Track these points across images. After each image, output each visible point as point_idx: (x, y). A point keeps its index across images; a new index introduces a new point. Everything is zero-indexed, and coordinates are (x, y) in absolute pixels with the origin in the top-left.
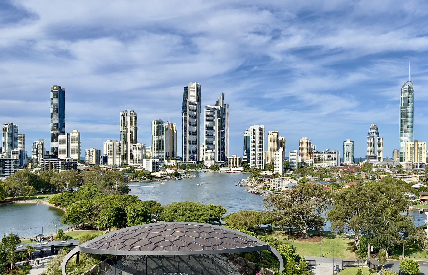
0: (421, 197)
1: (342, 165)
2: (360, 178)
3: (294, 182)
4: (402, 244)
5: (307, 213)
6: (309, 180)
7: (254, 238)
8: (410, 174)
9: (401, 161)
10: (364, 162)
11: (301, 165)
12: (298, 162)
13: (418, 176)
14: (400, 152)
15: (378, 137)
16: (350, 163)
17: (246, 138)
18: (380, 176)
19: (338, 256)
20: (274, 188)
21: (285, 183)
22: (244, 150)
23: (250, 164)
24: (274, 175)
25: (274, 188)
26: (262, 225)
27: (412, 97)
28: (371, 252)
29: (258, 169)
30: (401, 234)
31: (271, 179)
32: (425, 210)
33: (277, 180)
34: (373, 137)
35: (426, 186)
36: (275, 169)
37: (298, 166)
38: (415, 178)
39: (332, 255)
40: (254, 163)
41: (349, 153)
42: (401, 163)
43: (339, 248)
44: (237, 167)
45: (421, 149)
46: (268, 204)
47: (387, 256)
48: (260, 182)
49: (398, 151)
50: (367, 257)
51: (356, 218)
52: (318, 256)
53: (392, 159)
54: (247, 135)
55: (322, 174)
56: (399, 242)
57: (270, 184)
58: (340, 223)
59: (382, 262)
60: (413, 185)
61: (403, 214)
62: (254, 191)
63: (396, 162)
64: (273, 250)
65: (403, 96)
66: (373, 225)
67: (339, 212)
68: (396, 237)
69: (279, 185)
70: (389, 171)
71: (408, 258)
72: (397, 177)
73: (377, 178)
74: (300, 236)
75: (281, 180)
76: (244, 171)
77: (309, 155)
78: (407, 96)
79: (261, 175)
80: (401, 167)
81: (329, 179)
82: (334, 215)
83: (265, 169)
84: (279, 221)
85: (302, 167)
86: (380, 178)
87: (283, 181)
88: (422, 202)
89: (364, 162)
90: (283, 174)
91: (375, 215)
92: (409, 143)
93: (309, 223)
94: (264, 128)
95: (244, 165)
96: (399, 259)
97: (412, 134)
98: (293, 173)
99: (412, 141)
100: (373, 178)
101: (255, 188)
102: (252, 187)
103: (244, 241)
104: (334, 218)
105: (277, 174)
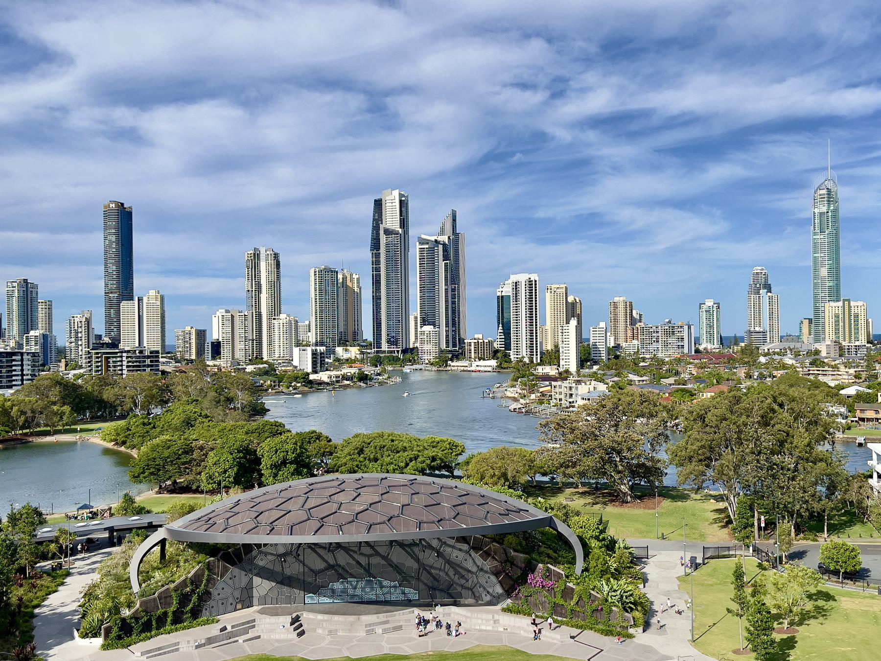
0: (859, 414)
1: (697, 351)
2: (734, 377)
3: (602, 387)
5: (629, 449)
7: (521, 504)
8: (835, 368)
9: (817, 340)
10: (743, 344)
11: (615, 352)
13: (852, 371)
14: (816, 322)
15: (769, 294)
18: (775, 373)
19: (694, 536)
20: (560, 400)
21: (583, 389)
23: (511, 352)
24: (560, 374)
25: (560, 400)
26: (539, 478)
27: (836, 211)
28: (760, 528)
31: (553, 383)
32: (869, 439)
33: (566, 384)
34: (759, 293)
36: (562, 363)
38: (845, 374)
40: (520, 351)
41: (711, 327)
42: (817, 346)
43: (696, 520)
44: (484, 360)
47: (793, 534)
49: (810, 321)
50: (754, 537)
51: (728, 458)
53: (798, 337)
54: (503, 294)
55: (657, 369)
57: (553, 394)
59: (784, 548)
64: (562, 528)
65: (817, 211)
67: (694, 447)
69: (571, 395)
70: (794, 362)
71: (835, 539)
72: (809, 374)
73: (770, 377)
74: (614, 497)
75: (574, 385)
76: (500, 366)
77: (629, 333)
78: (824, 209)
80: (817, 352)
81: (671, 380)
83: (542, 363)
86: (774, 377)
87: (579, 386)
89: (743, 344)
90: (578, 371)
92: (832, 304)
94: (537, 279)
97: (838, 286)
98: (599, 369)
99: (838, 301)
100: (762, 377)
101: (522, 401)
102: (515, 400)
103: (502, 510)
105: (567, 371)
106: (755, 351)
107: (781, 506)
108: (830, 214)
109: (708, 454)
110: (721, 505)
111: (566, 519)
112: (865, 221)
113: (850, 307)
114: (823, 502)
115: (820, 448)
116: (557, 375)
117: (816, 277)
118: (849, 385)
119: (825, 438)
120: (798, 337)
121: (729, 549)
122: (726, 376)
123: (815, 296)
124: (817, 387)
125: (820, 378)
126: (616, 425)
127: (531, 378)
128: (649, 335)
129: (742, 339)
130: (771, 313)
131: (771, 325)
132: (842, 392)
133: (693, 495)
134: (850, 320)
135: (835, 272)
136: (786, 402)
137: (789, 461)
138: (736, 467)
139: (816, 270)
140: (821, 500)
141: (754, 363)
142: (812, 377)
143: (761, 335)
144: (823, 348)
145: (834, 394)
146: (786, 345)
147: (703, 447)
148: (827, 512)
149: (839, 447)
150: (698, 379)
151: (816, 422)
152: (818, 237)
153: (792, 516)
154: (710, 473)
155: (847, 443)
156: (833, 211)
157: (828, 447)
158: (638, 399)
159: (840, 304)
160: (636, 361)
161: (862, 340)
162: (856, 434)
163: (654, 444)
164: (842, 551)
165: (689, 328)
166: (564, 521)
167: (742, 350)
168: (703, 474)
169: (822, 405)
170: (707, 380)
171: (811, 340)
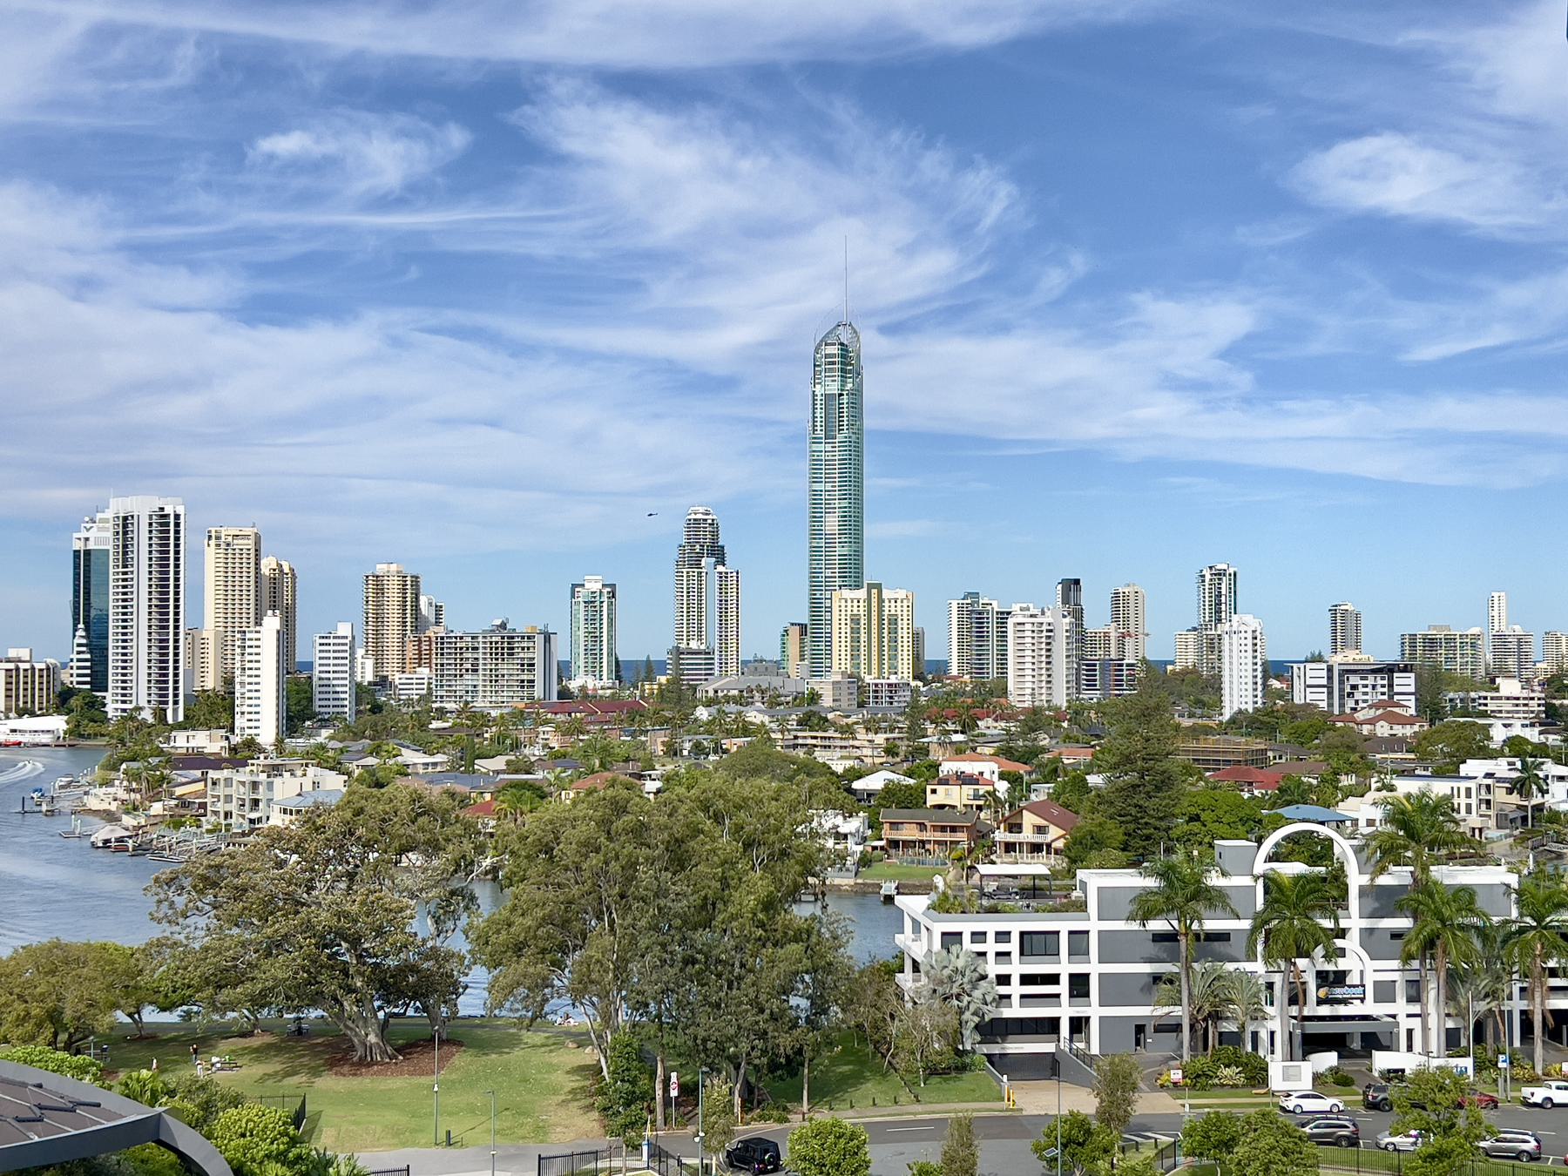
0: (887, 833)
1: (564, 694)
2: (640, 754)
3: (334, 782)
4: (800, 1052)
5: (379, 932)
6: (403, 771)
7: (87, 1088)
8: (848, 731)
9: (815, 673)
10: (663, 679)
11: (371, 698)
12: (359, 685)
13: (880, 739)
14: (812, 632)
15: (720, 568)
16: (598, 683)
17: (85, 565)
18: (726, 743)
19: (521, 1132)
20: (228, 815)
21: (286, 788)
22: (76, 622)
23: (109, 696)
24: (234, 749)
25: (228, 815)
26: (150, 1015)
27: (857, 393)
28: (667, 1101)
29: (151, 720)
30: (799, 1002)
31: (213, 774)
32: (905, 886)
33: (244, 775)
34: (698, 566)
35: (911, 781)
36: (239, 722)
37: (358, 701)
38: (870, 744)
39: (496, 1132)
40: (131, 691)
41: (595, 638)
42: (815, 684)
43: (530, 1092)
44: (33, 714)
45: (894, 621)
46: (180, 901)
47: (737, 1109)
48: (157, 787)
49: (803, 628)
50: (653, 1122)
51: (602, 943)
52: (426, 1145)
53: (778, 664)
54: (91, 546)
55: (469, 739)
56: (785, 1042)
57: (208, 800)
58: (531, 970)
59: (714, 1143)
60: (860, 777)
61: (803, 911)
62: (120, 840)
63: (797, 676)
64: (189, 1141)
65: (819, 390)
66: (676, 970)
67: (528, 921)
68: (774, 1018)
69: (256, 802)
70: (766, 719)
71: (823, 1116)
72: (795, 746)
73: (716, 752)
74: (339, 1053)
75: (263, 777)
76: (75, 732)
77: (411, 650)
78: (834, 388)
79: (161, 753)
80: (814, 697)
81: (499, 763)
82: (503, 936)
83: (190, 723)
84: (235, 986)
85: (377, 709)
86: (725, 751)
87: (277, 781)
88: (892, 852)
89: (663, 679)
90: (279, 743)
91: (685, 922)
92: (846, 593)
93: (391, 985)
94: (181, 510)
95: (73, 702)
96: (787, 1120)
97: (858, 555)
98: (331, 738)
99: (858, 587)
100: (698, 749)
101: (128, 820)
102: (110, 817)
103: (25, 1106)
104: (494, 953)
105: (251, 745)
107: (710, 1045)
111: (202, 1122)
112: (946, 448)
113: (881, 601)
114: (796, 1033)
116: (225, 755)
118: (873, 770)
121: (596, 1155)
126: (351, 876)
127: (154, 761)
128: (450, 653)
129: (661, 667)
131: (723, 639)
132: (856, 785)
138: (621, 968)
140: (795, 1026)
142: (801, 753)
147: (547, 920)
153: (737, 1068)
156: (851, 393)
158: (404, 809)
160: (424, 718)
161: (905, 671)
162: (881, 876)
163: (443, 915)
164: (831, 1139)
165: (547, 638)
166: (196, 1125)
171: (805, 673)
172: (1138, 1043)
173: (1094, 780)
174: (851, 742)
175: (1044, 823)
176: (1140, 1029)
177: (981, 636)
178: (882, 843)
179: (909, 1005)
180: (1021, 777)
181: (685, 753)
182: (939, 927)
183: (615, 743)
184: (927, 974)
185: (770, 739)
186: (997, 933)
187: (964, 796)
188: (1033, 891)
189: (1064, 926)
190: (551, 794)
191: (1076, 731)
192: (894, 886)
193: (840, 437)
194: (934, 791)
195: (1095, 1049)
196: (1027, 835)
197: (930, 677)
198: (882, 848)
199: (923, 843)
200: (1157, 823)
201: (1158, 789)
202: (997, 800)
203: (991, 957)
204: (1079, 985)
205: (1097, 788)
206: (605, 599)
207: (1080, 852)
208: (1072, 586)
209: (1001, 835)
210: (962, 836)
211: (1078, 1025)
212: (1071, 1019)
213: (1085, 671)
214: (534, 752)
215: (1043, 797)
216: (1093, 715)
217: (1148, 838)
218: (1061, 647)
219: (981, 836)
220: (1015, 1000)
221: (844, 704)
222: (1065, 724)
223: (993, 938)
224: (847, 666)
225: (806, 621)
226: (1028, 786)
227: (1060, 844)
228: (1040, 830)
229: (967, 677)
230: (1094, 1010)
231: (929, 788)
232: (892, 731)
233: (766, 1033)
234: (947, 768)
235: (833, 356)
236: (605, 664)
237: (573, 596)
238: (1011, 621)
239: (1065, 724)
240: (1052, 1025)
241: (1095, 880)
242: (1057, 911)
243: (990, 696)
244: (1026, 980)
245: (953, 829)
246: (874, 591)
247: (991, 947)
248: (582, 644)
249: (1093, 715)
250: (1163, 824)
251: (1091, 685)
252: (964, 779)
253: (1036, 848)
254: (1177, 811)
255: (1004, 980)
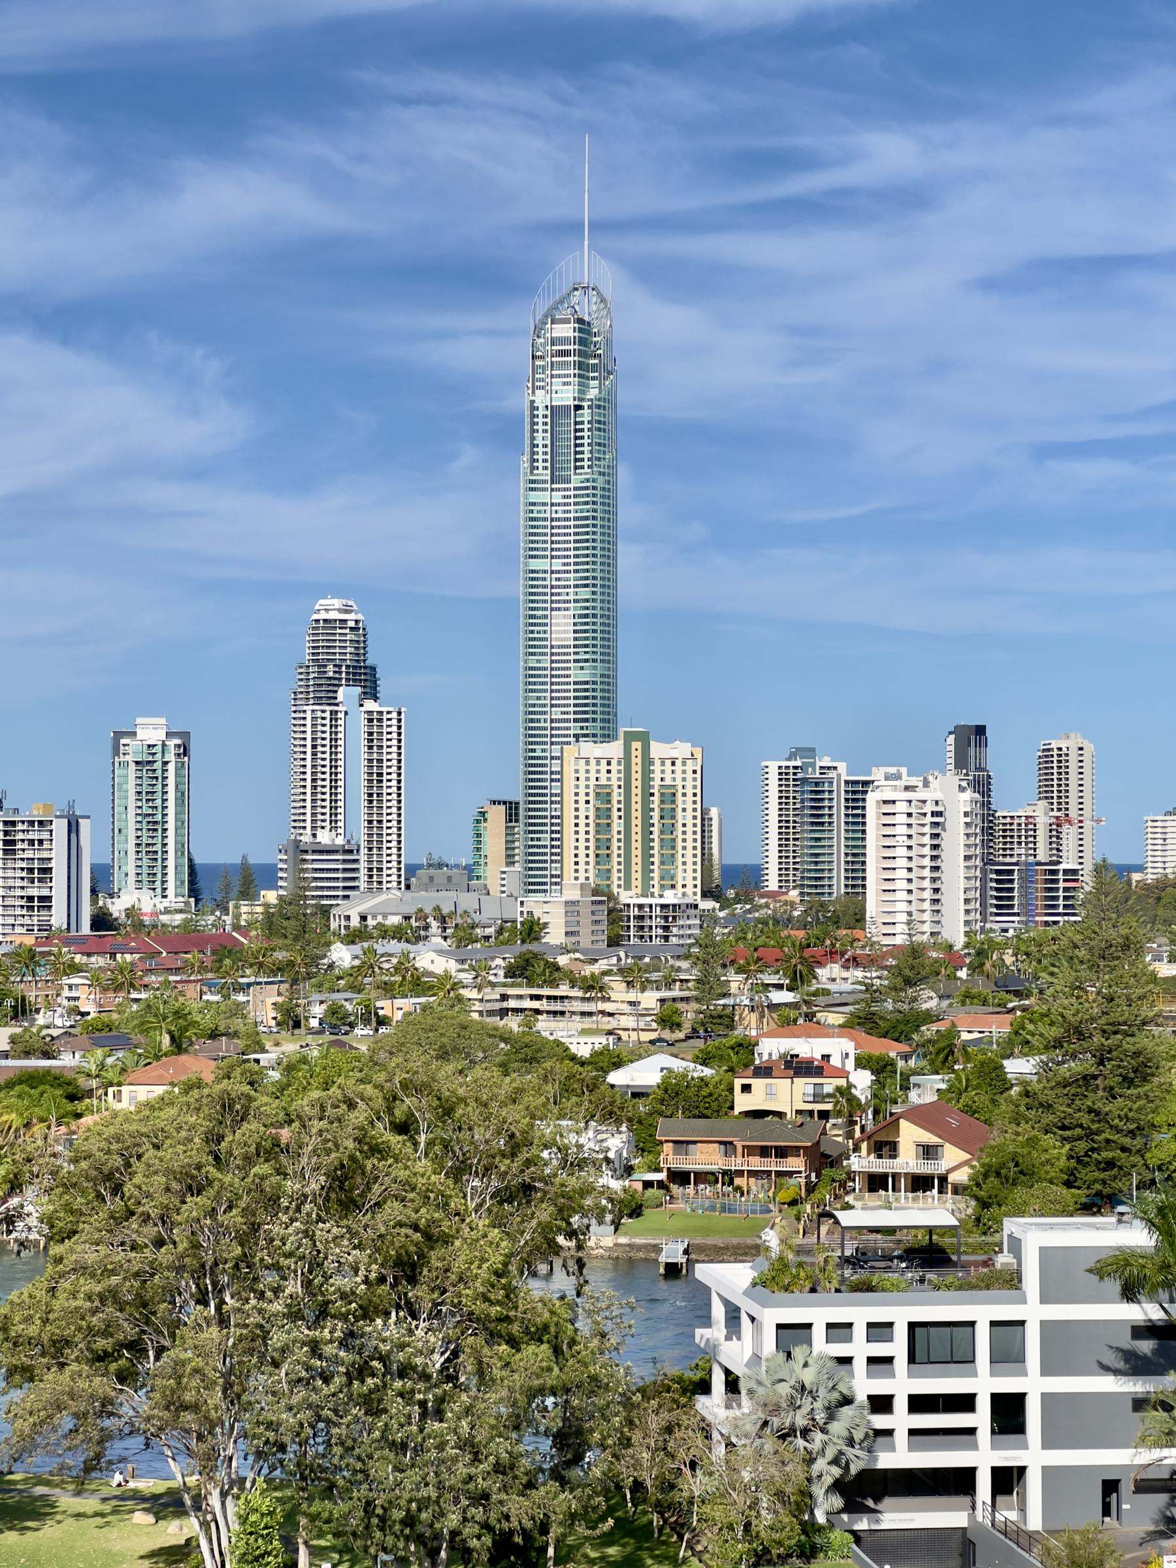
1: (101, 921)
2: (237, 1024)
8: (593, 987)
9: (532, 886)
10: (271, 896)
13: (650, 999)
15: (370, 705)
18: (385, 1007)
32: (701, 1249)
34: (332, 700)
35: (707, 1072)
38: (631, 1007)
41: (153, 824)
42: (536, 905)
45: (669, 797)
49: (512, 811)
51: (201, 1341)
58: (82, 1384)
63: (499, 893)
65: (541, 399)
70: (452, 966)
73: (366, 1021)
78: (566, 396)
80: (533, 929)
86: (382, 1022)
88: (675, 1189)
89: (271, 896)
92: (589, 749)
97: (608, 682)
100: (337, 1021)
106: (315, 924)
108: (586, 415)
109: (128, 1331)
110: (175, 1531)
112: (713, 442)
113: (647, 762)
114: (537, 1495)
115: (535, 1289)
117: (533, 646)
118: (638, 1054)
119: (556, 1249)
120: (471, 872)
122: (206, 1021)
123: (531, 717)
124: (531, 1060)
125: (544, 1025)
129: (269, 876)
130: (376, 778)
132: (616, 1078)
133: (66, 1501)
134: (647, 810)
135: (601, 630)
136: (424, 1119)
137: (426, 1344)
139: (534, 620)
141: (302, 971)
142: (513, 1024)
143: (335, 862)
144: (551, 911)
145: (585, 1085)
146: (426, 899)
147: (110, 1296)
148: (555, 1531)
149: (599, 1281)
150: (102, 1033)
151: (527, 1189)
152: (543, 497)
154: (135, 1403)
155: (628, 1265)
157: (563, 1282)
159: (614, 749)
161: (686, 887)
162: (660, 1231)
165: (73, 827)
167: (269, 916)
168: (107, 1408)
169: (545, 1128)
170: (138, 1038)
171: (514, 883)
172: (1106, 1511)
173: (1018, 1067)
174: (602, 1006)
175: (933, 1139)
176: (1110, 1487)
177: (819, 821)
178: (662, 1176)
179: (720, 1450)
180: (892, 1064)
181: (314, 1023)
182: (774, 1316)
183: (195, 1006)
184: (751, 1392)
185: (460, 999)
186: (870, 1325)
187: (798, 1097)
188: (929, 1255)
189: (982, 1312)
190: (90, 1093)
191: (981, 986)
192: (681, 1247)
193: (576, 481)
194: (746, 1088)
195: (1035, 1523)
196: (907, 1161)
197: (731, 894)
198: (661, 1185)
199: (729, 1176)
200: (1127, 1141)
201: (1128, 1081)
202: (852, 1100)
203: (860, 1365)
204: (1009, 1413)
205: (1024, 1083)
206: (171, 757)
207: (997, 1189)
208: (973, 737)
209: (862, 1162)
210: (796, 1163)
211: (1007, 1480)
212: (995, 1471)
213: (998, 887)
214: (51, 1021)
215: (930, 1098)
216: (1009, 959)
217: (1110, 1164)
218: (957, 841)
219: (823, 1160)
220: (901, 1437)
221: (585, 940)
222: (963, 974)
223: (863, 1332)
224: (591, 874)
225: (518, 795)
226: (905, 1077)
227: (961, 1176)
228: (928, 1152)
229: (794, 894)
230: (1032, 1455)
231: (738, 1083)
232: (669, 986)
233: (486, 1496)
234: (770, 1048)
235: (566, 341)
236: (171, 870)
237: (116, 752)
238: (872, 798)
239: (963, 974)
240: (959, 1482)
241: (1037, 1236)
242: (972, 1287)
243: (835, 922)
244: (919, 1404)
245: (782, 1153)
246: (636, 745)
247: (860, 1348)
248: (132, 834)
249: (1009, 959)
250: (1138, 1143)
251: (1004, 907)
252: (797, 1067)
253: (920, 1183)
254: (1158, 1120)
255: (882, 1404)
